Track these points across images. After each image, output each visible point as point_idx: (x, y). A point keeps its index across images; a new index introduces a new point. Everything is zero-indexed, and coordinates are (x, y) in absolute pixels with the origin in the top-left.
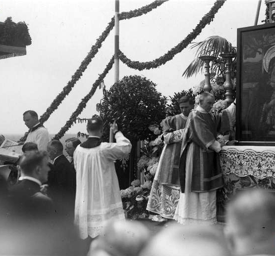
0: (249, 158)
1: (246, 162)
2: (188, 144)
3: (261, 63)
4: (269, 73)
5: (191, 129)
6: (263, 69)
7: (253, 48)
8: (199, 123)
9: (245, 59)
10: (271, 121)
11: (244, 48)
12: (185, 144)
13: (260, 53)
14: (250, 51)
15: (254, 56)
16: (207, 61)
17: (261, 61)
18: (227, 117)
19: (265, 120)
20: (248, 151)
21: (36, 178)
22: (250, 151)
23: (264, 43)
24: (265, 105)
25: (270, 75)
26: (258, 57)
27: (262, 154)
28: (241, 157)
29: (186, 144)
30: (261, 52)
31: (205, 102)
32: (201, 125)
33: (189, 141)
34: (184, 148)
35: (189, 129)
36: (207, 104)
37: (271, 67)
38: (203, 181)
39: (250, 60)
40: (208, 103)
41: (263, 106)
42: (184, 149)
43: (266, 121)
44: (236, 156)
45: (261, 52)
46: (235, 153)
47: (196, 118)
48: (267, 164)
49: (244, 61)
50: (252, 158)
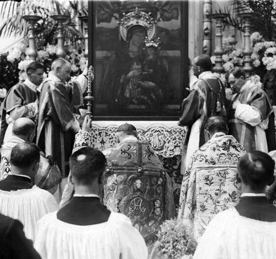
0: (112, 134)
1: (108, 140)
2: (47, 122)
3: (117, 30)
4: (127, 42)
5: (50, 104)
6: (120, 37)
7: (107, 12)
8: (58, 98)
9: (99, 23)
10: (130, 94)
11: (96, 11)
12: (42, 122)
13: (116, 19)
14: (103, 15)
15: (109, 21)
16: (32, 22)
17: (118, 28)
18: (78, 90)
19: (123, 92)
20: (112, 127)
21: (96, 194)
22: (114, 126)
23: (121, 8)
24: (123, 77)
25: (129, 44)
26: (114, 23)
27: (107, 129)
28: (103, 134)
29: (44, 123)
30: (118, 17)
31: (63, 70)
32: (61, 101)
33: (46, 119)
34: (42, 127)
35: (47, 104)
36: (65, 73)
37: (129, 35)
38: (64, 165)
39: (104, 25)
40: (67, 72)
41: (121, 77)
42: (41, 129)
43: (125, 94)
44: (97, 132)
45: (118, 17)
46: (96, 130)
47: (55, 91)
48: (112, 140)
49: (97, 25)
50: (94, 134)
